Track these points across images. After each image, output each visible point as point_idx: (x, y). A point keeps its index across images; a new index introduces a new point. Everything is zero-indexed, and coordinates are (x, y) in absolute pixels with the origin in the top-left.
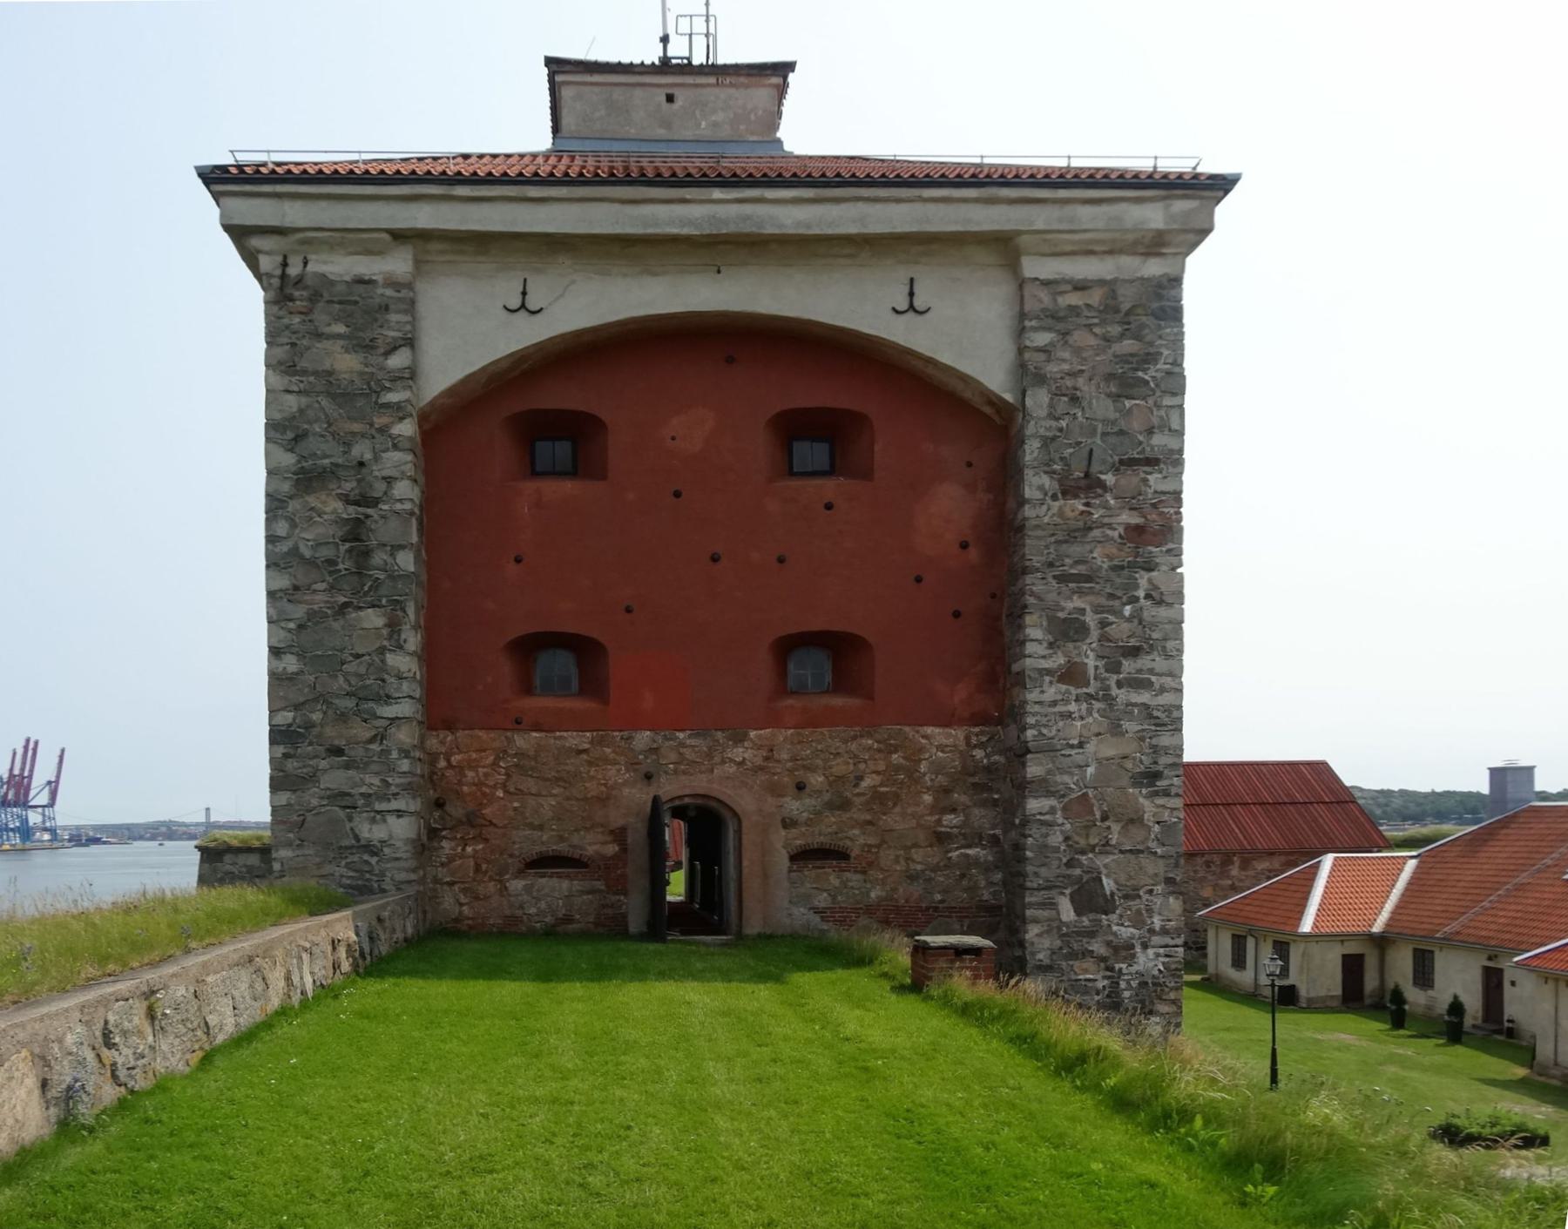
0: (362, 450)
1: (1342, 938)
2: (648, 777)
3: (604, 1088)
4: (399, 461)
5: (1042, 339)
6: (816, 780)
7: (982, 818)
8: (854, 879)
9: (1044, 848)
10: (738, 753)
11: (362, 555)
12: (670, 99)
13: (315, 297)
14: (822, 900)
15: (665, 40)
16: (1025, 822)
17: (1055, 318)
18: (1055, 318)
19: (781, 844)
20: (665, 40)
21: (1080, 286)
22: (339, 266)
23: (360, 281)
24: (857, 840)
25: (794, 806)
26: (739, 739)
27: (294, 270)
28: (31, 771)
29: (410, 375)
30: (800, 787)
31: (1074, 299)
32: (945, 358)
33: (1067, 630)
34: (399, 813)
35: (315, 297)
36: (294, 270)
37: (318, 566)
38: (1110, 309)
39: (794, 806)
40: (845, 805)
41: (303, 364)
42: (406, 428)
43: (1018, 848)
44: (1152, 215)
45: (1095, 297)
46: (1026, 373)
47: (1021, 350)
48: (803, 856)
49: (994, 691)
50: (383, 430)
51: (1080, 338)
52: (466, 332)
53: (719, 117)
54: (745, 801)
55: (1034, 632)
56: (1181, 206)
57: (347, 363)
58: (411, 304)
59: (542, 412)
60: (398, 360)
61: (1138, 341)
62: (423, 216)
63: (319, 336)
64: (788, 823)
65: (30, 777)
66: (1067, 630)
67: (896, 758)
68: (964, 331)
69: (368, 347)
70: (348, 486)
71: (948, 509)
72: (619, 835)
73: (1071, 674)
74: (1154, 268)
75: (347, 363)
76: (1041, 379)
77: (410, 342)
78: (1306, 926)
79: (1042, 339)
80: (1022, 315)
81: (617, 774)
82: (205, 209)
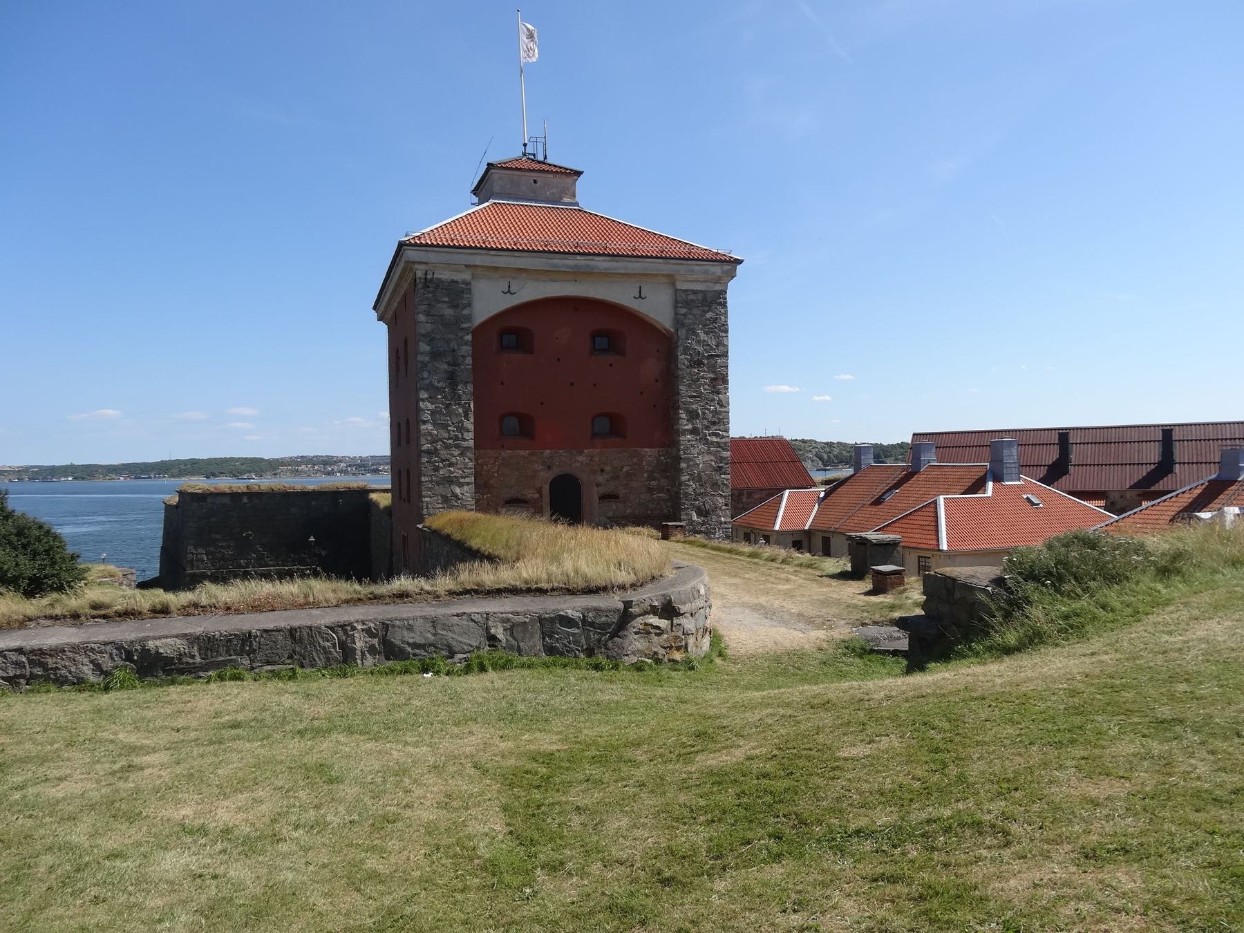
0: (453, 345)
1: (792, 533)
2: (549, 467)
4: (466, 349)
5: (683, 311)
6: (608, 468)
7: (664, 482)
8: (621, 506)
9: (687, 494)
10: (580, 458)
12: (535, 182)
13: (437, 286)
14: (610, 514)
15: (525, 145)
16: (680, 484)
17: (688, 304)
18: (688, 304)
19: (595, 493)
20: (525, 145)
21: (695, 292)
22: (446, 275)
23: (453, 281)
24: (622, 492)
25: (600, 479)
26: (581, 453)
27: (429, 277)
29: (469, 318)
30: (602, 471)
31: (692, 297)
32: (651, 315)
33: (693, 415)
34: (468, 484)
35: (437, 286)
36: (429, 277)
37: (1031, 575)
38: (705, 299)
39: (600, 479)
40: (618, 478)
41: (433, 312)
42: (469, 337)
43: (677, 493)
44: (717, 270)
45: (700, 297)
46: (678, 322)
47: (676, 314)
48: (603, 497)
49: (668, 437)
50: (461, 338)
51: (695, 311)
53: (554, 190)
54: (584, 477)
56: (727, 267)
57: (448, 312)
60: (465, 312)
61: (716, 301)
62: (479, 260)
63: (439, 302)
64: (598, 485)
66: (693, 415)
67: (635, 460)
68: (657, 308)
69: (455, 307)
70: (449, 359)
71: (651, 367)
73: (694, 431)
74: (718, 287)
76: (683, 325)
77: (469, 305)
78: (777, 528)
79: (683, 311)
80: (676, 302)
81: (538, 467)
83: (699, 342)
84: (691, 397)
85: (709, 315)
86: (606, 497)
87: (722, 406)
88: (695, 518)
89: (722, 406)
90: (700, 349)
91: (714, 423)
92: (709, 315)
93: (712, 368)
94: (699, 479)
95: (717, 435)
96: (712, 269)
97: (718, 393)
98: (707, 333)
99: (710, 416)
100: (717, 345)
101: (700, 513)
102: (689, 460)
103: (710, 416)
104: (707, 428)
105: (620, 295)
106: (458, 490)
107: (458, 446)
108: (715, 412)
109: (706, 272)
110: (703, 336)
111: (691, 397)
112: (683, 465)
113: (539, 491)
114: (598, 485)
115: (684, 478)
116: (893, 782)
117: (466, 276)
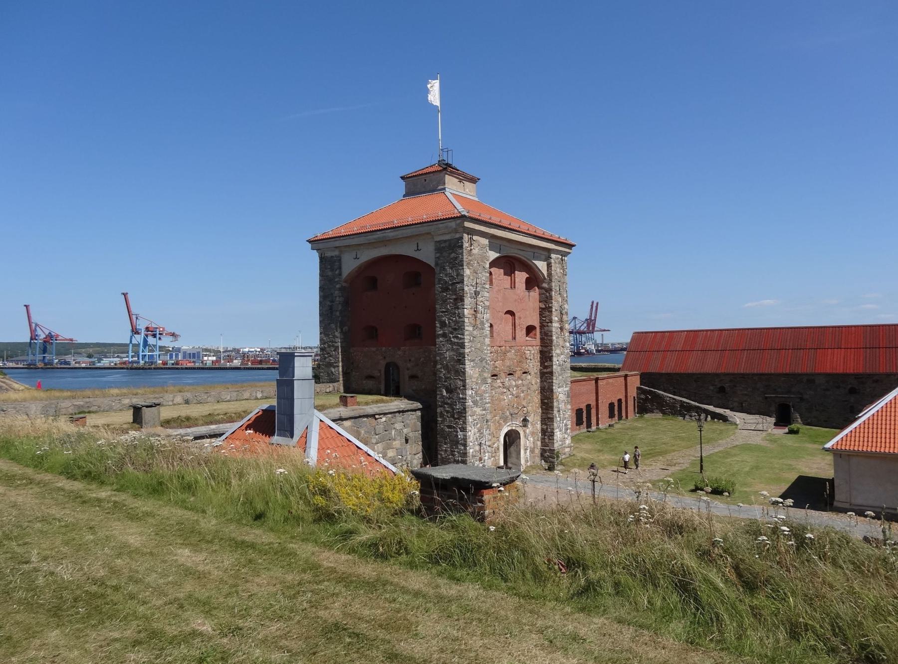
3: (756, 539)
6: (413, 359)
10: (399, 353)
11: (332, 313)
14: (414, 388)
21: (445, 241)
25: (409, 365)
26: (399, 349)
28: (595, 317)
33: (443, 325)
39: (409, 365)
45: (447, 244)
46: (437, 264)
52: (349, 265)
55: (438, 325)
56: (458, 221)
58: (340, 260)
59: (370, 276)
62: (337, 244)
64: (408, 369)
65: (595, 320)
68: (427, 254)
72: (380, 371)
73: (444, 335)
75: (330, 273)
82: (309, 245)
83: (446, 275)
84: (443, 312)
85: (453, 255)
86: (413, 377)
87: (460, 317)
88: (445, 393)
89: (460, 317)
90: (447, 279)
91: (455, 329)
92: (453, 255)
93: (455, 292)
94: (446, 367)
95: (457, 337)
96: (450, 224)
97: (458, 308)
98: (451, 268)
99: (453, 324)
100: (457, 275)
101: (449, 391)
102: (441, 354)
103: (453, 324)
104: (452, 333)
105: (407, 250)
106: (333, 370)
107: (333, 346)
108: (456, 322)
109: (447, 227)
110: (449, 271)
111: (443, 312)
112: (438, 358)
113: (380, 371)
114: (408, 369)
115: (439, 366)
116: (210, 522)
117: (336, 253)
